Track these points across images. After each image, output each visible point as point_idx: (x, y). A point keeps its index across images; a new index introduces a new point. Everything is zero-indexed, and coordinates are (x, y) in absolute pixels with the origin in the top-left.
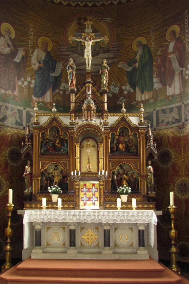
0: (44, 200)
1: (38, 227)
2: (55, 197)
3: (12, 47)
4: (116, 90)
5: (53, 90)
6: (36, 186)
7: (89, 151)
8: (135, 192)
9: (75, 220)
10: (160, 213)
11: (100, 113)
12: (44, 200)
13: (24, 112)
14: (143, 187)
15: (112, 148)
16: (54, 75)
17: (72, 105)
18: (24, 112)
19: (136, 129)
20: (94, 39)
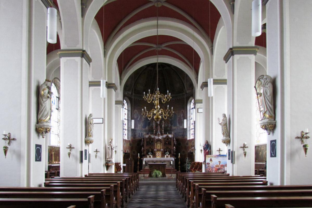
0: (148, 156)
1: (147, 162)
2: (150, 155)
3: (137, 116)
4: (167, 126)
5: (148, 126)
6: (145, 153)
7: (158, 144)
8: (170, 153)
9: (155, 160)
10: (176, 158)
11: (162, 134)
12: (148, 156)
13: (140, 133)
14: (172, 152)
15: (165, 143)
17: (154, 133)
18: (140, 133)
19: (171, 138)
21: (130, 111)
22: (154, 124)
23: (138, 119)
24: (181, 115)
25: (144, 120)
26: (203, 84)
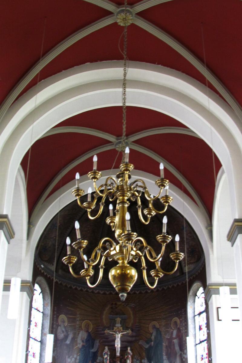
3: (65, 333)
16: (93, 350)
20: (122, 332)
21: (49, 318)
22: (106, 356)
23: (68, 342)
24: (172, 333)
25: (83, 346)
26: (236, 224)
